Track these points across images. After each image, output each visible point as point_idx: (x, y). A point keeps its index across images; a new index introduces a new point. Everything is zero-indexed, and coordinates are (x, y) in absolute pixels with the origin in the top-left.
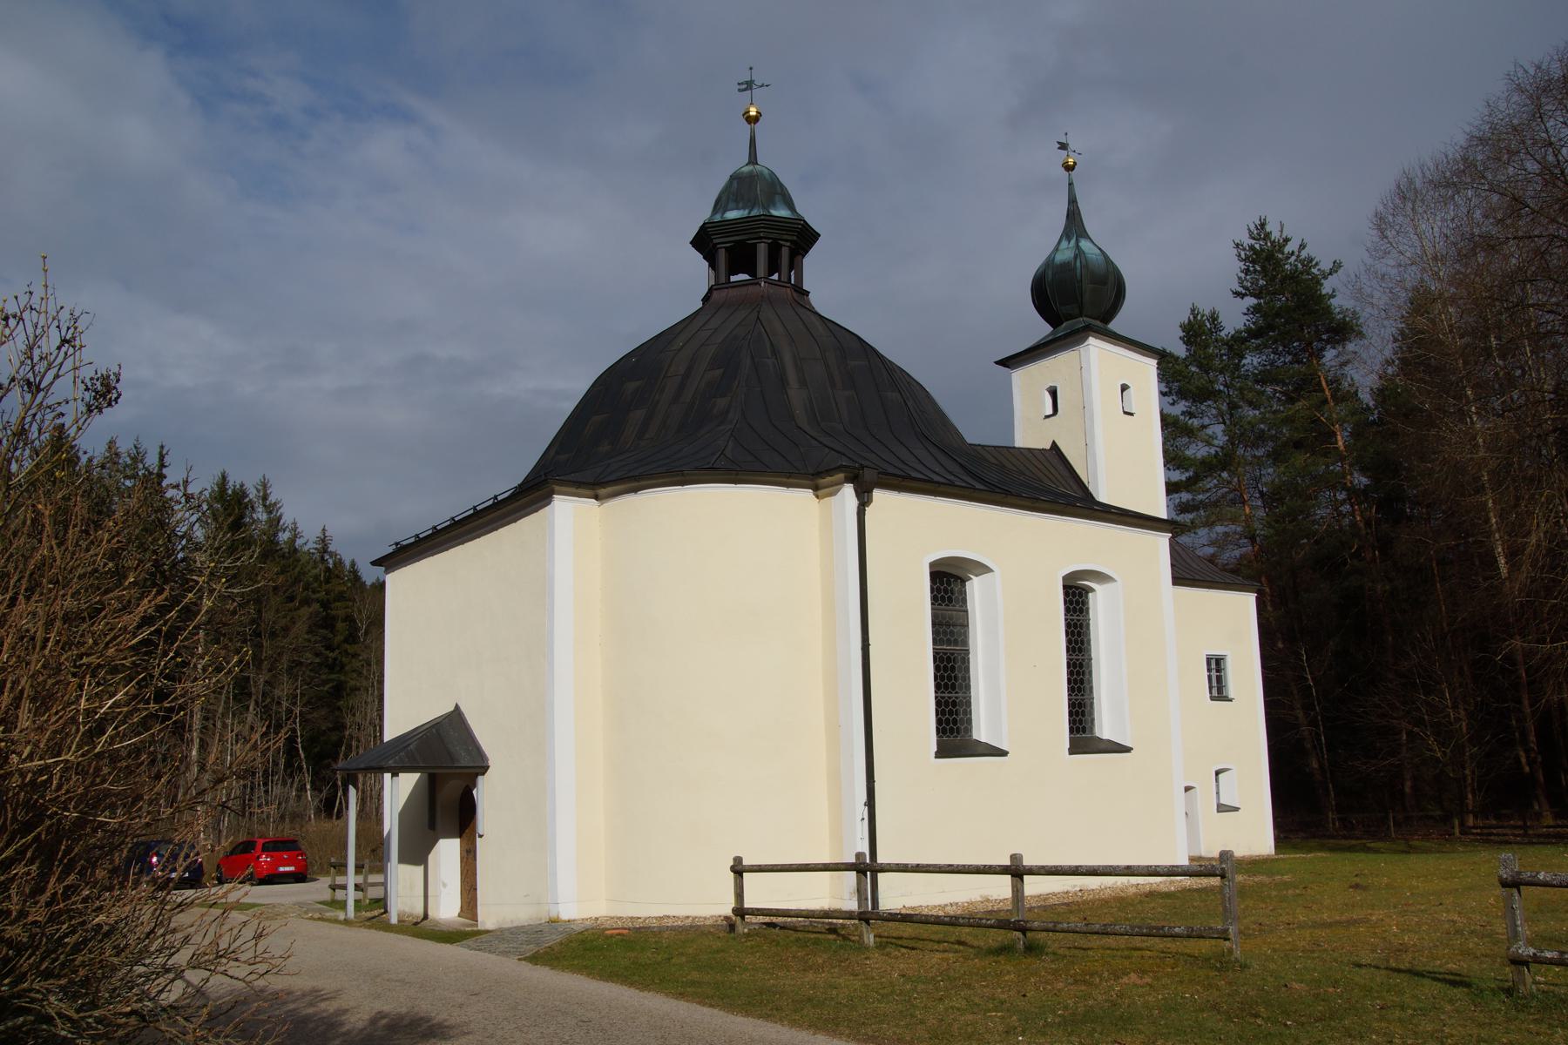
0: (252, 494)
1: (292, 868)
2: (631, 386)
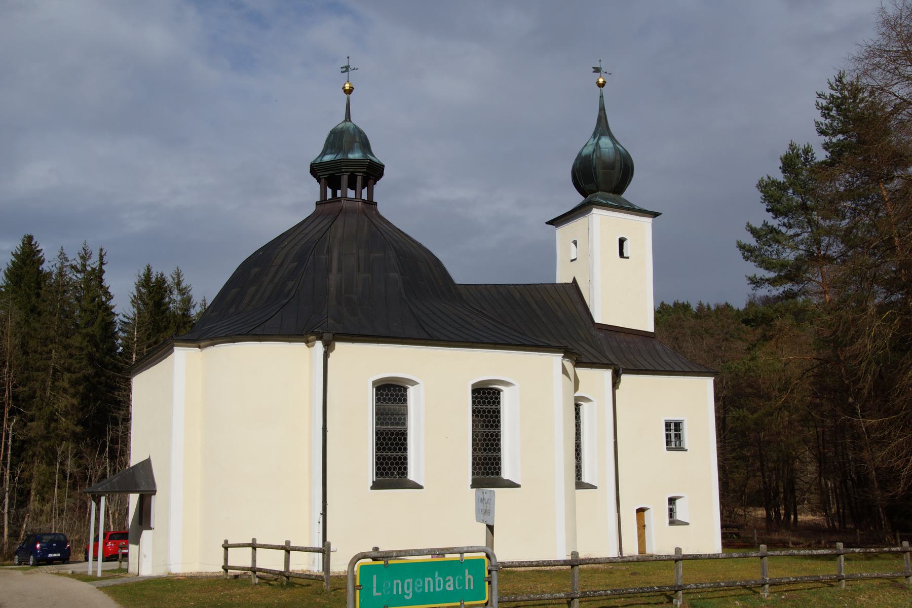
0: (170, 281)
1: (59, 555)
2: (255, 270)
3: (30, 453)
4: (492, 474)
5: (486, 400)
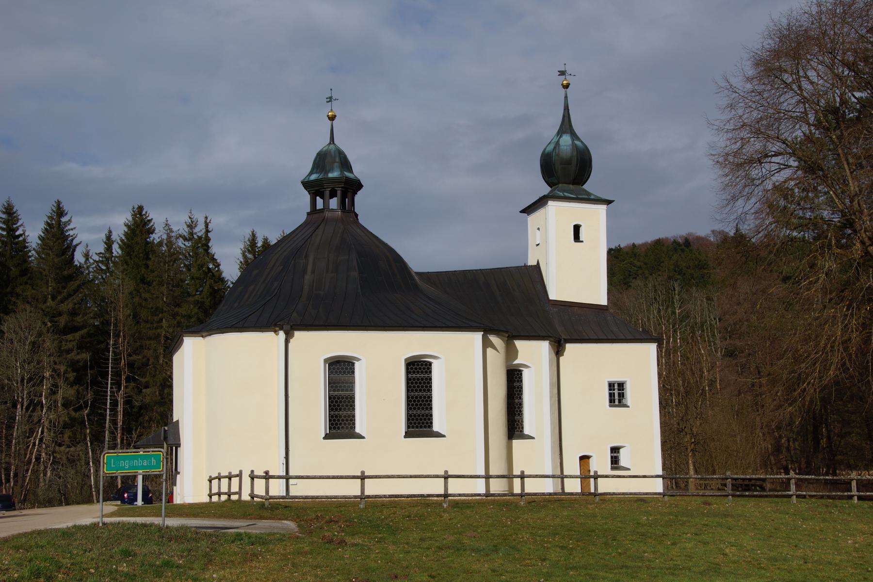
3: (147, 418)
4: (425, 427)
5: (418, 374)
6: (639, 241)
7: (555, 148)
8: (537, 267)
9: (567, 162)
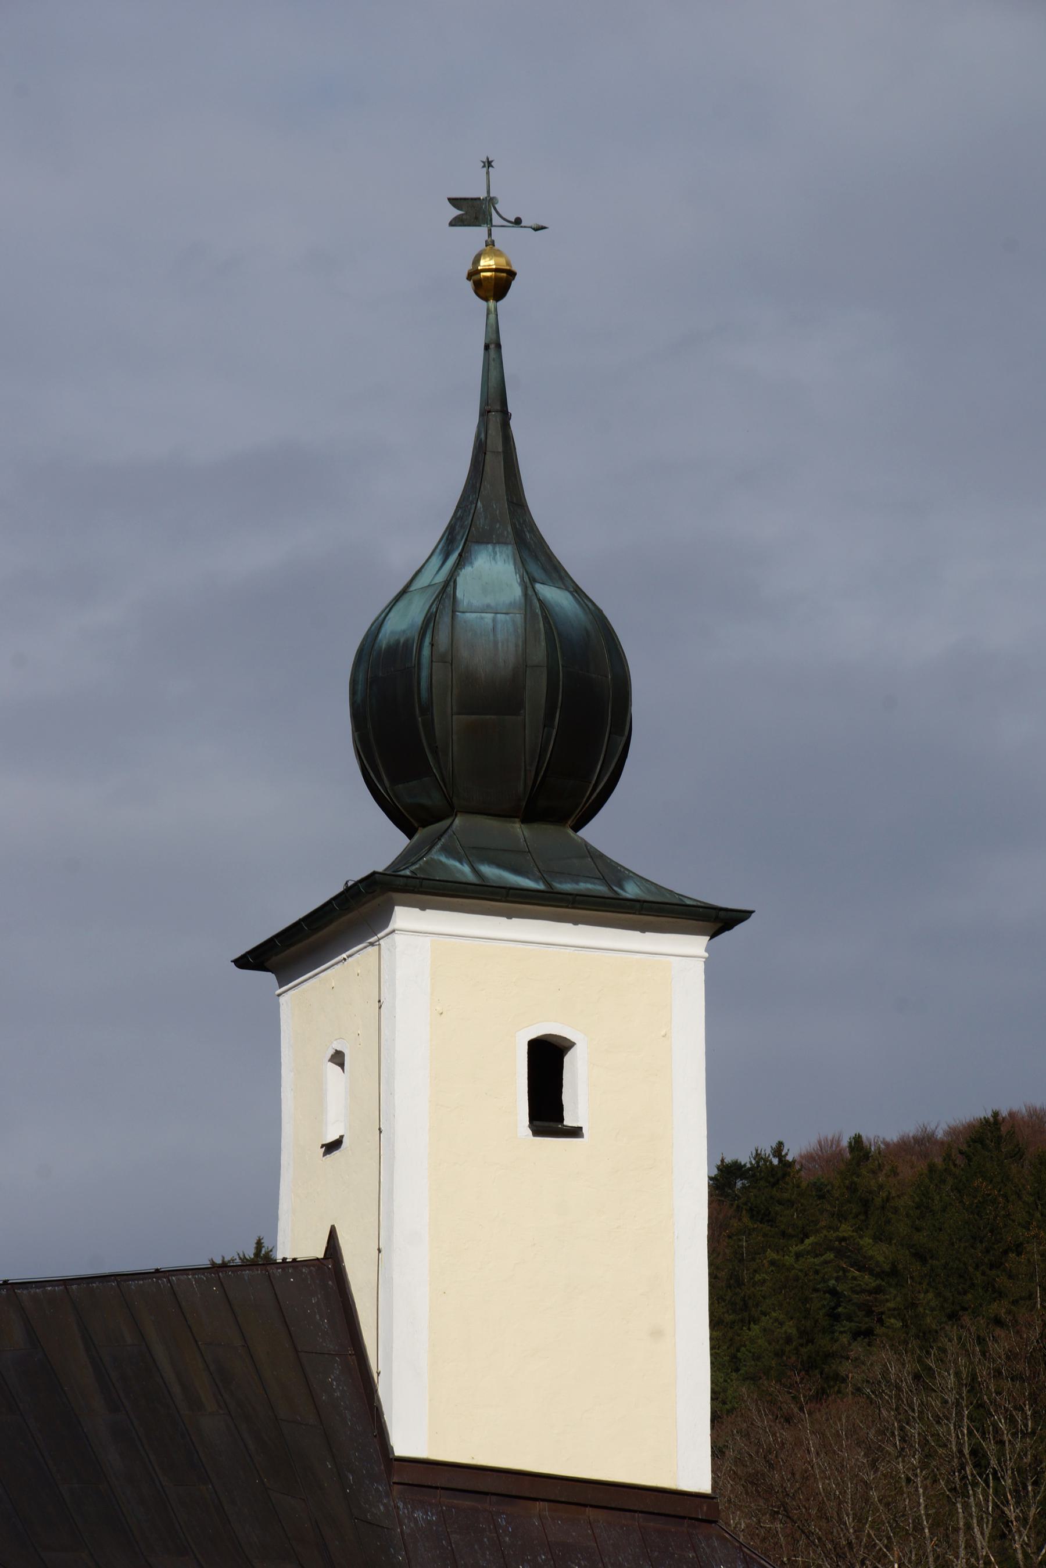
6: (885, 1128)
7: (430, 621)
8: (331, 1263)
9: (493, 699)
